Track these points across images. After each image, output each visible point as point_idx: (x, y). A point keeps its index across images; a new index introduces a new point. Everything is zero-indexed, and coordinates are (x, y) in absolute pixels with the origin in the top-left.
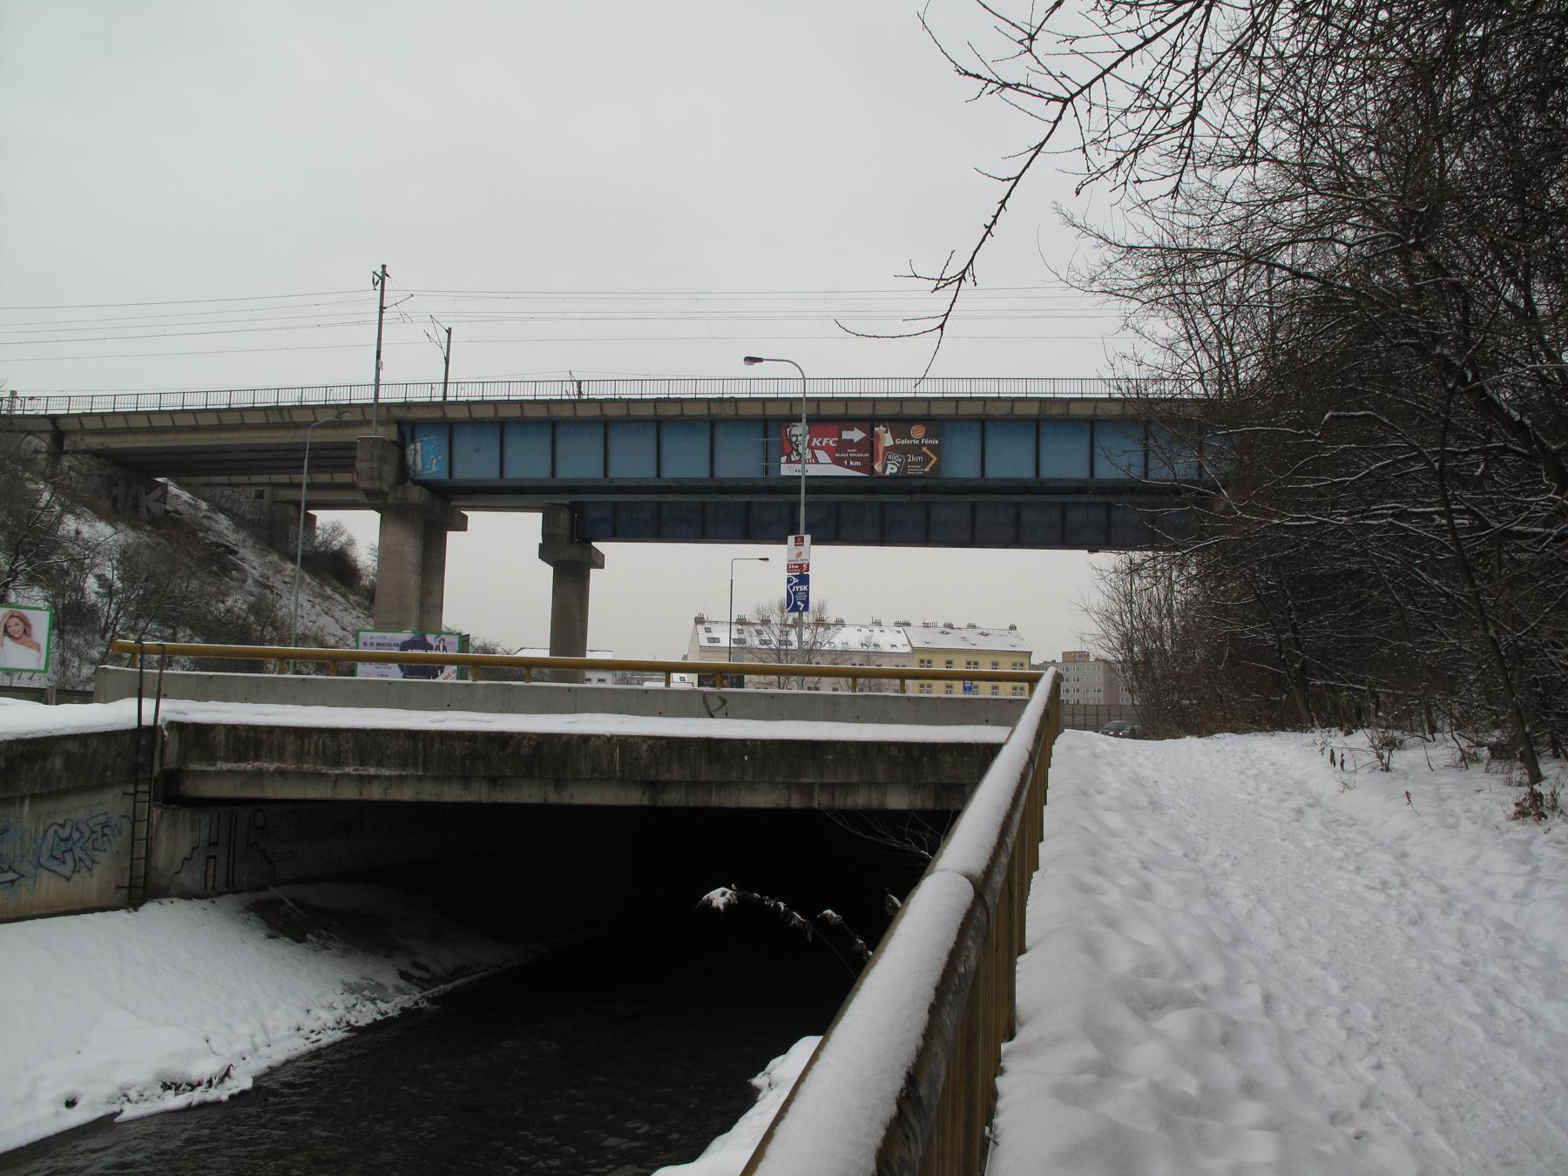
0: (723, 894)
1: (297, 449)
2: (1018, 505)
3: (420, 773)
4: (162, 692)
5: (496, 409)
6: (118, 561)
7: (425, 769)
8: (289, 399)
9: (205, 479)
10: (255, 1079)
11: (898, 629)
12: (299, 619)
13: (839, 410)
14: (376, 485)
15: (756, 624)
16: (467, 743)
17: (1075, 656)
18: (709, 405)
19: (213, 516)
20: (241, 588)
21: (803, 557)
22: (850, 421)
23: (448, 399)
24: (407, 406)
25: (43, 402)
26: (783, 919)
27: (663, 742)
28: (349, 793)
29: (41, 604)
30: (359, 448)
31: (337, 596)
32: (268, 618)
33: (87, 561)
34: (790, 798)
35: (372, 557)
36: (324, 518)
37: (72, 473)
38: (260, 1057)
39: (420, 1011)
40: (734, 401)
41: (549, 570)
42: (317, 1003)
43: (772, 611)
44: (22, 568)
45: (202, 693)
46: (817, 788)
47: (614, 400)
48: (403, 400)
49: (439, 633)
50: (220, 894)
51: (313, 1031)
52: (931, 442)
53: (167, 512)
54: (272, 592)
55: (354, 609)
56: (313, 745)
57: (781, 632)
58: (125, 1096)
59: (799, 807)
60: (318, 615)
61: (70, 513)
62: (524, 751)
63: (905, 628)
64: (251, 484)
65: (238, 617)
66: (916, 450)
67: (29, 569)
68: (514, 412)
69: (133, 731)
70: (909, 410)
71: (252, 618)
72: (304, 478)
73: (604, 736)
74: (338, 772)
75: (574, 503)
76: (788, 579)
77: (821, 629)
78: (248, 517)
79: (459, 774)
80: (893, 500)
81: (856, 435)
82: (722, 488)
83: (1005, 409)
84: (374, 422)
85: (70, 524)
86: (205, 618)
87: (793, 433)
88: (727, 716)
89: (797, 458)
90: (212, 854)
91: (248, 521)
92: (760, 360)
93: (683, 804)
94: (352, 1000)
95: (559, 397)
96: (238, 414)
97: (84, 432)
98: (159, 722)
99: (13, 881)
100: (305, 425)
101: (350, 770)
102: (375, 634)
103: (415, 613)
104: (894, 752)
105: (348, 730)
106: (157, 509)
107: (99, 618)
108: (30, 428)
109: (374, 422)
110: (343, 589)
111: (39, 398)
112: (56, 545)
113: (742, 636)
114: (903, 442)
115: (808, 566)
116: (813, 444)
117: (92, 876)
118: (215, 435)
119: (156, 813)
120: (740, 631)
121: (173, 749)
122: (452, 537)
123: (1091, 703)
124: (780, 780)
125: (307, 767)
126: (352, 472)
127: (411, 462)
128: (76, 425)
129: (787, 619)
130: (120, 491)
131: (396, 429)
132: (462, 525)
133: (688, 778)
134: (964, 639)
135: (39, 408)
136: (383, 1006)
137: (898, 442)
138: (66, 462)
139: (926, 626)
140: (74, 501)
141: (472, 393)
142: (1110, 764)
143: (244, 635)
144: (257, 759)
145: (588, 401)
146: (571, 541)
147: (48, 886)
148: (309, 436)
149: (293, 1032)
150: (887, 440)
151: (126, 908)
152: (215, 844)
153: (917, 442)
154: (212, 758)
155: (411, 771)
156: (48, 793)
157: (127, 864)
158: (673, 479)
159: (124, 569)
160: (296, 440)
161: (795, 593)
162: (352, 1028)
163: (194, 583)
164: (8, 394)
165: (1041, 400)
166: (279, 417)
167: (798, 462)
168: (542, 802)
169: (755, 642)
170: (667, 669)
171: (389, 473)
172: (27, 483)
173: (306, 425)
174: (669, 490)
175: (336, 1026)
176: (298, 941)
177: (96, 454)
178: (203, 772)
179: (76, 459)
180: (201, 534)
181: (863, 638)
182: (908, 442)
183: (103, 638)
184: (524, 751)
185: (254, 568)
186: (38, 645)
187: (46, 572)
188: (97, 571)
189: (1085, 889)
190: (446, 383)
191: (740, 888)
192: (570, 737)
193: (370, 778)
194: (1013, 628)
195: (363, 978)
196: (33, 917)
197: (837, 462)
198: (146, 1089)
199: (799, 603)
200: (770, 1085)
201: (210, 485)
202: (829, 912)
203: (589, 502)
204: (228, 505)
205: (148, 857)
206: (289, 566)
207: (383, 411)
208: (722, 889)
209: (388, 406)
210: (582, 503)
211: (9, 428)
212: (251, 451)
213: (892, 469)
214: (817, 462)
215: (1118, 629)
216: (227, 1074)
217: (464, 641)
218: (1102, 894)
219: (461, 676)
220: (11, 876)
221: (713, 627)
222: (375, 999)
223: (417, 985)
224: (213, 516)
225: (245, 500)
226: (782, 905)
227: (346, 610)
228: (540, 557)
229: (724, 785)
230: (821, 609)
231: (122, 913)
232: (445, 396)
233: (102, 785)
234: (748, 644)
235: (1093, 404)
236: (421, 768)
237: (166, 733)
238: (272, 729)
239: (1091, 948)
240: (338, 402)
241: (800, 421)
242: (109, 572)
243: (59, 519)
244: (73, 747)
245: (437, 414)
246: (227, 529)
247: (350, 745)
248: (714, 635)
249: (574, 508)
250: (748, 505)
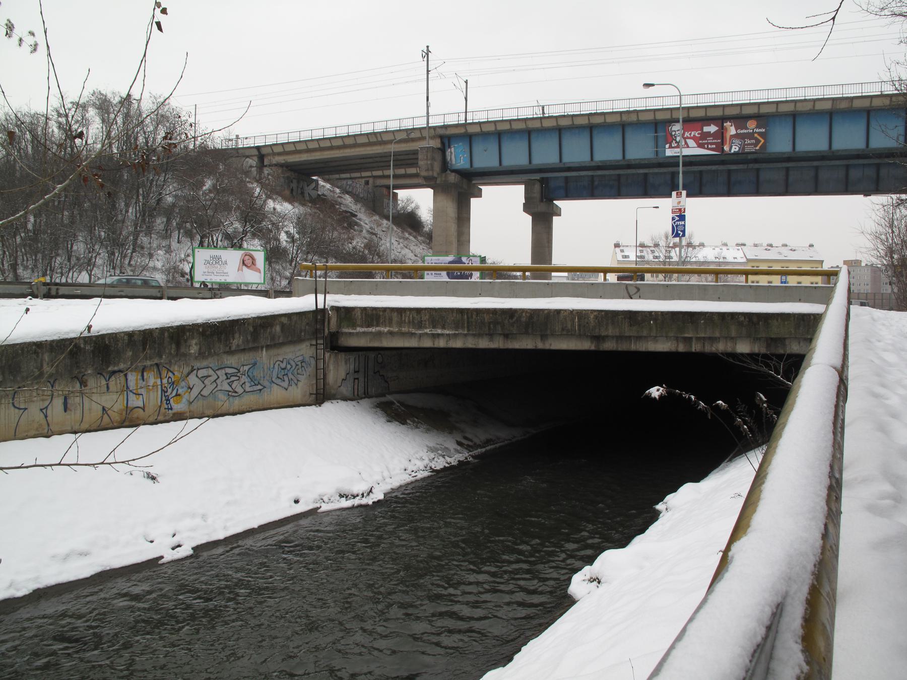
0: (658, 390)
1: (387, 156)
2: (817, 168)
3: (466, 332)
4: (327, 291)
5: (496, 125)
6: (296, 224)
7: (468, 330)
8: (379, 128)
9: (337, 176)
10: (385, 494)
11: (738, 248)
12: (392, 251)
13: (701, 114)
14: (430, 173)
15: (650, 247)
16: (491, 315)
17: (852, 263)
18: (621, 115)
19: (343, 196)
20: (360, 235)
21: (681, 204)
22: (708, 120)
23: (468, 122)
24: (445, 127)
25: (252, 139)
26: (692, 406)
27: (603, 313)
28: (427, 343)
29: (259, 248)
30: (419, 152)
31: (411, 238)
32: (376, 250)
33: (281, 224)
34: (678, 346)
35: (430, 215)
36: (402, 194)
37: (270, 177)
38: (386, 483)
39: (468, 463)
40: (636, 112)
41: (529, 218)
42: (414, 457)
43: (661, 239)
44: (249, 229)
45: (347, 290)
46: (694, 340)
47: (564, 116)
48: (443, 124)
49: (469, 256)
50: (361, 399)
51: (413, 471)
52: (760, 130)
53: (319, 195)
54: (377, 236)
55: (421, 244)
56: (407, 318)
57: (666, 251)
58: (322, 499)
59: (684, 351)
60: (402, 248)
61: (270, 198)
62: (523, 319)
63: (742, 247)
64: (362, 177)
65: (359, 251)
66: (750, 136)
67: (252, 230)
68: (507, 127)
69: (313, 312)
70: (747, 111)
71: (366, 252)
72: (391, 172)
73: (569, 310)
74: (421, 332)
75: (543, 179)
76: (673, 218)
77: (690, 249)
78: (361, 195)
79: (487, 332)
81: (712, 129)
82: (630, 166)
83: (809, 107)
84: (427, 138)
85: (271, 204)
86: (342, 252)
87: (673, 129)
88: (640, 297)
89: (676, 145)
90: (356, 377)
91: (361, 198)
92: (653, 85)
93: (615, 349)
94: (432, 455)
95: (532, 117)
96: (353, 138)
97: (274, 154)
98: (326, 307)
99: (260, 390)
100: (390, 142)
101: (427, 331)
102: (434, 258)
103: (455, 245)
104: (742, 319)
105: (426, 309)
106: (314, 194)
107: (288, 255)
108: (247, 154)
109: (427, 138)
110: (414, 234)
111: (250, 138)
112: (264, 216)
113: (642, 254)
114: (742, 131)
115: (685, 209)
116: (685, 136)
117: (298, 387)
118: (342, 151)
119: (327, 355)
120: (641, 251)
121: (334, 321)
122: (473, 201)
123: (862, 291)
124: (672, 335)
125: (405, 329)
126: (416, 167)
127: (449, 159)
128: (269, 150)
129: (670, 243)
130: (294, 185)
131: (439, 141)
132: (479, 194)
133: (618, 334)
134: (780, 253)
135: (250, 143)
136: (449, 460)
137: (739, 131)
138: (266, 171)
139: (756, 245)
140: (272, 192)
141: (481, 117)
142: (884, 325)
143: (363, 259)
144: (378, 325)
145: (549, 117)
146: (542, 201)
147: (276, 393)
148: (392, 148)
149: (403, 471)
150: (732, 131)
151: (315, 405)
152: (358, 372)
153: (751, 131)
154: (354, 326)
155: (460, 331)
156: (274, 345)
157: (315, 382)
158: (601, 162)
159: (299, 228)
160: (385, 151)
161: (677, 226)
162: (433, 471)
163: (336, 234)
164: (235, 137)
165: (833, 99)
166: (375, 138)
167: (678, 147)
168: (534, 348)
169: (650, 257)
170: (605, 271)
171: (437, 167)
172: (248, 184)
173: (390, 142)
174: (598, 168)
175: (424, 469)
176: (403, 424)
177: (281, 165)
178: (350, 333)
179: (271, 169)
180: (338, 207)
181: (716, 253)
182: (745, 131)
183: (291, 265)
184: (523, 319)
185: (367, 224)
186: (259, 270)
187: (261, 231)
188: (286, 229)
189: (876, 396)
190: (466, 112)
191: (668, 386)
192: (549, 311)
193: (439, 335)
194: (811, 246)
195: (438, 444)
196: (271, 409)
197: (701, 146)
198: (331, 496)
199: (679, 232)
200: (667, 509)
201: (340, 179)
202: (720, 402)
203: (551, 177)
204: (350, 190)
205: (324, 378)
206: (385, 222)
207: (432, 131)
208: (657, 387)
209: (435, 128)
210: (547, 178)
211: (237, 155)
212: (361, 159)
213: (735, 149)
214: (688, 147)
215: (883, 244)
216: (371, 491)
217: (483, 260)
218: (887, 399)
219: (482, 277)
220: (259, 387)
221: (625, 249)
222: (444, 455)
223: (466, 449)
224: (343, 196)
225: (359, 186)
226: (693, 397)
227: (417, 245)
228: (525, 211)
229: (639, 338)
230: (690, 238)
231: (314, 407)
232: (466, 120)
233: (300, 340)
234: (646, 259)
235: (870, 99)
236: (466, 330)
237: (330, 312)
238: (385, 310)
239: (883, 429)
240: (406, 128)
241: (678, 122)
242: (292, 230)
243: (265, 201)
244: (285, 320)
245: (462, 131)
246: (351, 203)
247: (427, 317)
248: (626, 253)
249: (542, 181)
250: (646, 175)
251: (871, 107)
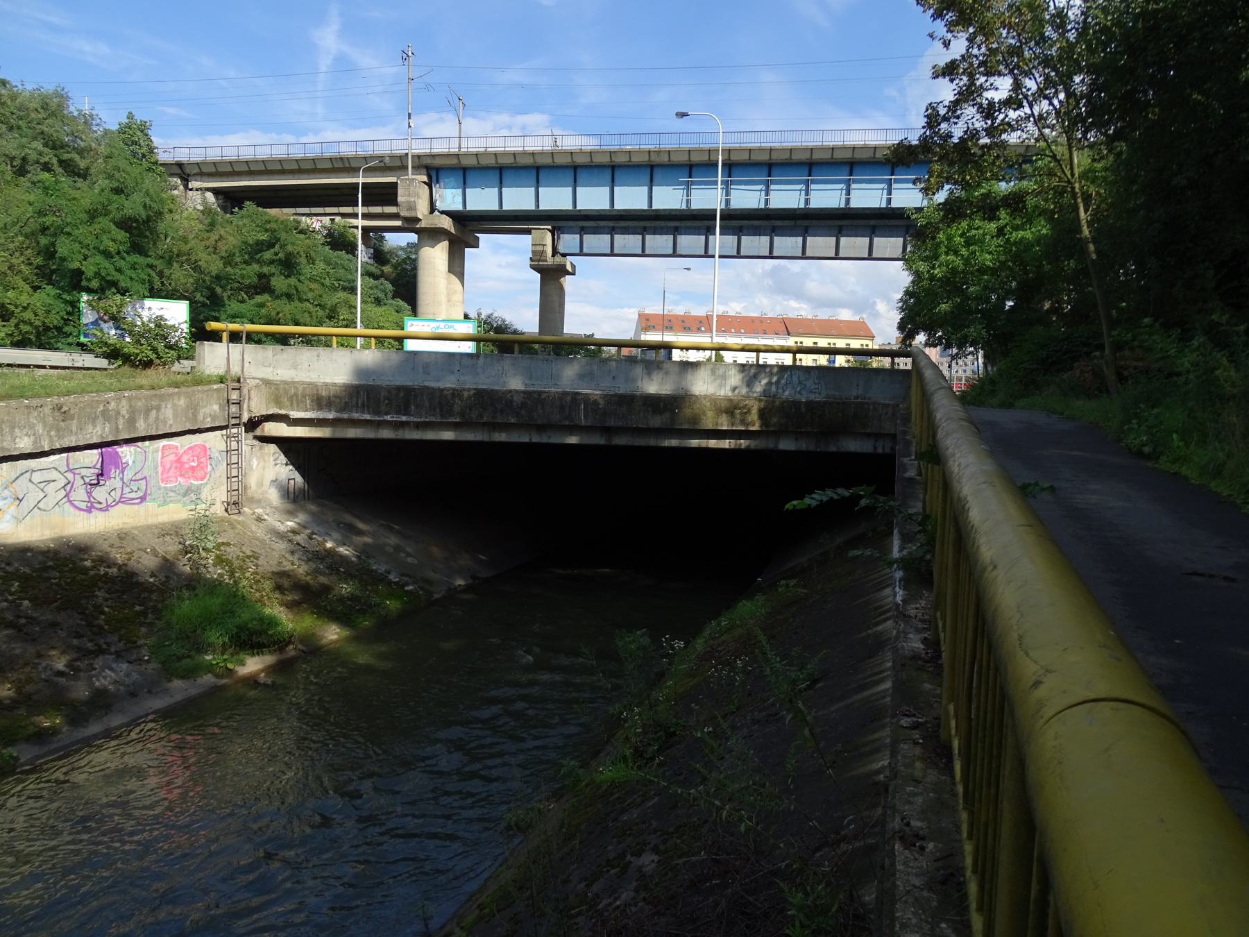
23: (462, 150)
68: (510, 161)
72: (360, 210)
80: (782, 224)
101: (388, 418)
245: (455, 161)
251: (853, 158)
